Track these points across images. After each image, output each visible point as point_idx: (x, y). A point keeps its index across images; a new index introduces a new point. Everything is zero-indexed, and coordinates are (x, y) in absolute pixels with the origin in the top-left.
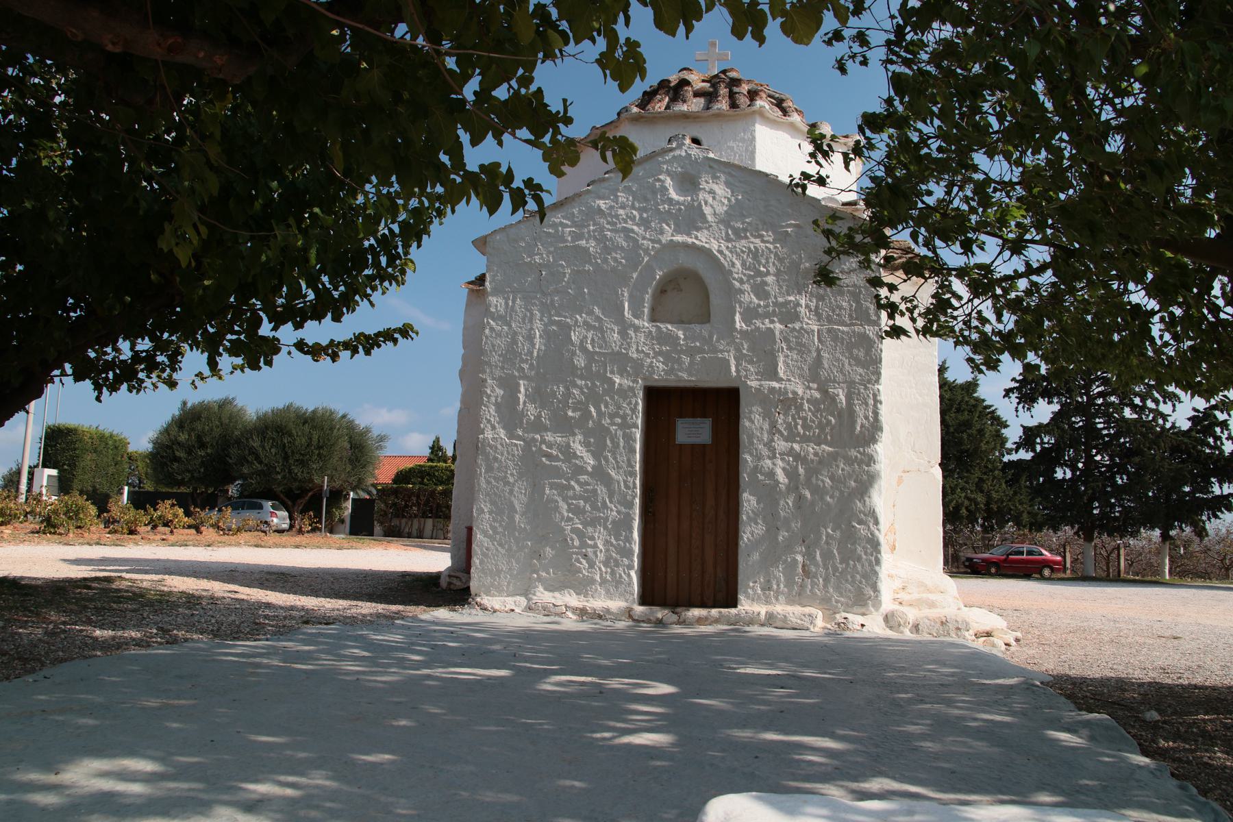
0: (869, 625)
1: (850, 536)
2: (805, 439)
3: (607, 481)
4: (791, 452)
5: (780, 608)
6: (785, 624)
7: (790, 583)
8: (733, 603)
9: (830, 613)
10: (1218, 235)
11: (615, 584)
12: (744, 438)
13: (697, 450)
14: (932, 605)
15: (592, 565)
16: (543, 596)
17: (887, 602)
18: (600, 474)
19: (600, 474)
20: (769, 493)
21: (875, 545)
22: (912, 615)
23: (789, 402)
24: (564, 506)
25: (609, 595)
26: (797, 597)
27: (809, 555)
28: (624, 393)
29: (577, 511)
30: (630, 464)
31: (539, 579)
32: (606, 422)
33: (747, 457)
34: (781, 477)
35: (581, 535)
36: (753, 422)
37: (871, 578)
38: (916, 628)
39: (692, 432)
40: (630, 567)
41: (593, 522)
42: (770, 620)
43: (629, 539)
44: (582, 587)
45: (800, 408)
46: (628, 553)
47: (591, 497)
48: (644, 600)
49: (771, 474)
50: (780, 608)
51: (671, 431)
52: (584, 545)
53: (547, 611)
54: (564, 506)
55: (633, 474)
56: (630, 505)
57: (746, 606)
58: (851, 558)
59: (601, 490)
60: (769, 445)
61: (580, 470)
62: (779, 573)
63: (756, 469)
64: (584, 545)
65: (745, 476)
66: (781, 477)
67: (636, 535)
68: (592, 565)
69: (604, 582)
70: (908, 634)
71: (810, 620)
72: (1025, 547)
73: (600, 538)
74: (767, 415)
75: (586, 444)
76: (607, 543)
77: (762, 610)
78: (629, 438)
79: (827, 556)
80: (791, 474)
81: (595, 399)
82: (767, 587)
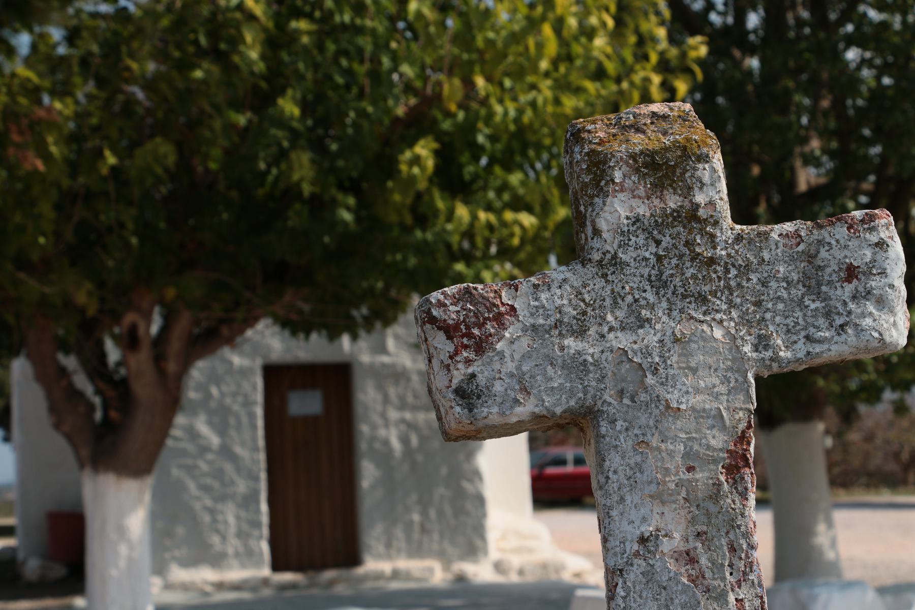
0: (481, 572)
1: (459, 495)
2: (415, 409)
3: (233, 458)
4: (403, 421)
5: (403, 564)
6: (407, 576)
7: (409, 539)
8: (350, 556)
9: (447, 564)
10: (725, 27)
11: (248, 556)
12: (359, 410)
13: (310, 421)
14: (530, 551)
15: (224, 538)
16: (179, 574)
17: (494, 554)
18: (226, 452)
19: (226, 452)
20: (384, 458)
21: (480, 501)
22: (516, 561)
23: (398, 375)
24: (192, 486)
25: (243, 566)
26: (416, 551)
27: (424, 514)
28: (244, 373)
29: (206, 489)
30: (254, 439)
31: (174, 559)
32: (228, 401)
33: (364, 429)
34: (396, 444)
35: (212, 511)
36: (367, 395)
37: (479, 530)
38: (521, 572)
39: (305, 404)
40: (261, 537)
41: (223, 498)
42: (396, 575)
43: (258, 511)
44: (217, 560)
45: (408, 380)
46: (257, 525)
47: (219, 474)
48: (277, 567)
49: (386, 443)
50: (403, 564)
51: (284, 403)
52: (215, 521)
53: (185, 587)
54: (192, 486)
55: (256, 449)
56: (256, 479)
57: (375, 565)
58: (463, 523)
59: (229, 467)
60: (383, 415)
61: (204, 449)
62: (399, 532)
63: (373, 439)
64: (215, 521)
65: (363, 446)
66: (396, 444)
67: (264, 507)
68: (224, 538)
69: (237, 555)
70: (514, 578)
71: (435, 573)
72: (570, 453)
73: (230, 515)
74: (380, 388)
75: (210, 423)
76: (238, 518)
77: (386, 567)
78: (252, 416)
79: (441, 513)
80: (405, 440)
81: (217, 380)
82: (388, 545)
